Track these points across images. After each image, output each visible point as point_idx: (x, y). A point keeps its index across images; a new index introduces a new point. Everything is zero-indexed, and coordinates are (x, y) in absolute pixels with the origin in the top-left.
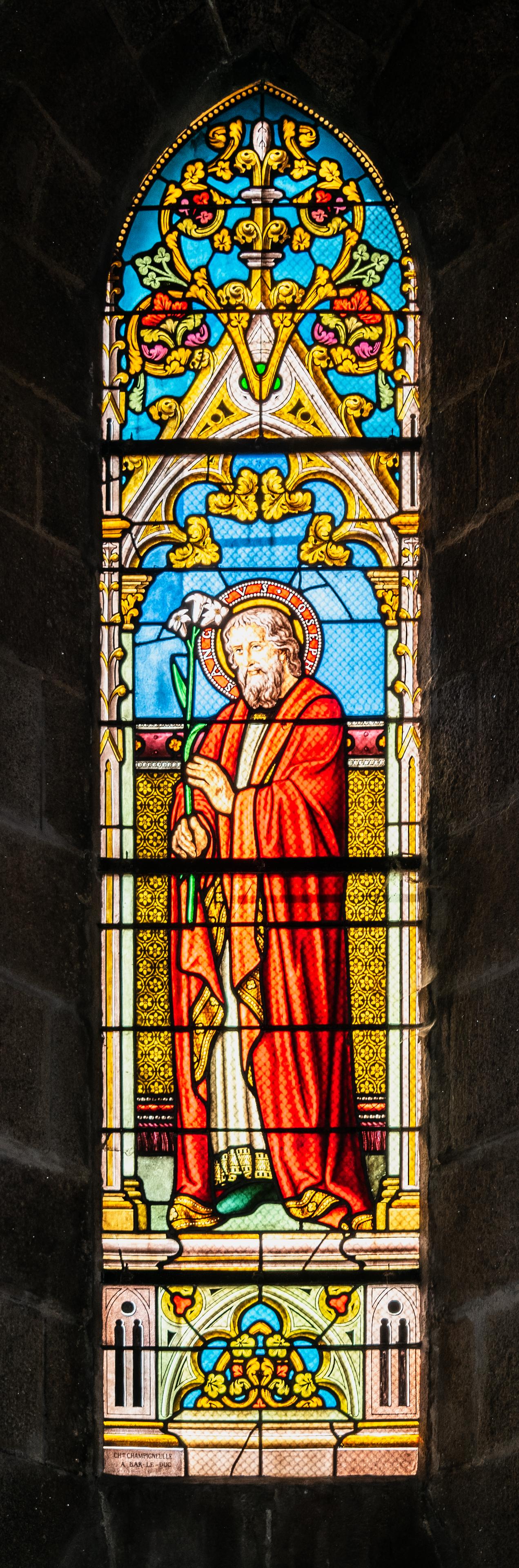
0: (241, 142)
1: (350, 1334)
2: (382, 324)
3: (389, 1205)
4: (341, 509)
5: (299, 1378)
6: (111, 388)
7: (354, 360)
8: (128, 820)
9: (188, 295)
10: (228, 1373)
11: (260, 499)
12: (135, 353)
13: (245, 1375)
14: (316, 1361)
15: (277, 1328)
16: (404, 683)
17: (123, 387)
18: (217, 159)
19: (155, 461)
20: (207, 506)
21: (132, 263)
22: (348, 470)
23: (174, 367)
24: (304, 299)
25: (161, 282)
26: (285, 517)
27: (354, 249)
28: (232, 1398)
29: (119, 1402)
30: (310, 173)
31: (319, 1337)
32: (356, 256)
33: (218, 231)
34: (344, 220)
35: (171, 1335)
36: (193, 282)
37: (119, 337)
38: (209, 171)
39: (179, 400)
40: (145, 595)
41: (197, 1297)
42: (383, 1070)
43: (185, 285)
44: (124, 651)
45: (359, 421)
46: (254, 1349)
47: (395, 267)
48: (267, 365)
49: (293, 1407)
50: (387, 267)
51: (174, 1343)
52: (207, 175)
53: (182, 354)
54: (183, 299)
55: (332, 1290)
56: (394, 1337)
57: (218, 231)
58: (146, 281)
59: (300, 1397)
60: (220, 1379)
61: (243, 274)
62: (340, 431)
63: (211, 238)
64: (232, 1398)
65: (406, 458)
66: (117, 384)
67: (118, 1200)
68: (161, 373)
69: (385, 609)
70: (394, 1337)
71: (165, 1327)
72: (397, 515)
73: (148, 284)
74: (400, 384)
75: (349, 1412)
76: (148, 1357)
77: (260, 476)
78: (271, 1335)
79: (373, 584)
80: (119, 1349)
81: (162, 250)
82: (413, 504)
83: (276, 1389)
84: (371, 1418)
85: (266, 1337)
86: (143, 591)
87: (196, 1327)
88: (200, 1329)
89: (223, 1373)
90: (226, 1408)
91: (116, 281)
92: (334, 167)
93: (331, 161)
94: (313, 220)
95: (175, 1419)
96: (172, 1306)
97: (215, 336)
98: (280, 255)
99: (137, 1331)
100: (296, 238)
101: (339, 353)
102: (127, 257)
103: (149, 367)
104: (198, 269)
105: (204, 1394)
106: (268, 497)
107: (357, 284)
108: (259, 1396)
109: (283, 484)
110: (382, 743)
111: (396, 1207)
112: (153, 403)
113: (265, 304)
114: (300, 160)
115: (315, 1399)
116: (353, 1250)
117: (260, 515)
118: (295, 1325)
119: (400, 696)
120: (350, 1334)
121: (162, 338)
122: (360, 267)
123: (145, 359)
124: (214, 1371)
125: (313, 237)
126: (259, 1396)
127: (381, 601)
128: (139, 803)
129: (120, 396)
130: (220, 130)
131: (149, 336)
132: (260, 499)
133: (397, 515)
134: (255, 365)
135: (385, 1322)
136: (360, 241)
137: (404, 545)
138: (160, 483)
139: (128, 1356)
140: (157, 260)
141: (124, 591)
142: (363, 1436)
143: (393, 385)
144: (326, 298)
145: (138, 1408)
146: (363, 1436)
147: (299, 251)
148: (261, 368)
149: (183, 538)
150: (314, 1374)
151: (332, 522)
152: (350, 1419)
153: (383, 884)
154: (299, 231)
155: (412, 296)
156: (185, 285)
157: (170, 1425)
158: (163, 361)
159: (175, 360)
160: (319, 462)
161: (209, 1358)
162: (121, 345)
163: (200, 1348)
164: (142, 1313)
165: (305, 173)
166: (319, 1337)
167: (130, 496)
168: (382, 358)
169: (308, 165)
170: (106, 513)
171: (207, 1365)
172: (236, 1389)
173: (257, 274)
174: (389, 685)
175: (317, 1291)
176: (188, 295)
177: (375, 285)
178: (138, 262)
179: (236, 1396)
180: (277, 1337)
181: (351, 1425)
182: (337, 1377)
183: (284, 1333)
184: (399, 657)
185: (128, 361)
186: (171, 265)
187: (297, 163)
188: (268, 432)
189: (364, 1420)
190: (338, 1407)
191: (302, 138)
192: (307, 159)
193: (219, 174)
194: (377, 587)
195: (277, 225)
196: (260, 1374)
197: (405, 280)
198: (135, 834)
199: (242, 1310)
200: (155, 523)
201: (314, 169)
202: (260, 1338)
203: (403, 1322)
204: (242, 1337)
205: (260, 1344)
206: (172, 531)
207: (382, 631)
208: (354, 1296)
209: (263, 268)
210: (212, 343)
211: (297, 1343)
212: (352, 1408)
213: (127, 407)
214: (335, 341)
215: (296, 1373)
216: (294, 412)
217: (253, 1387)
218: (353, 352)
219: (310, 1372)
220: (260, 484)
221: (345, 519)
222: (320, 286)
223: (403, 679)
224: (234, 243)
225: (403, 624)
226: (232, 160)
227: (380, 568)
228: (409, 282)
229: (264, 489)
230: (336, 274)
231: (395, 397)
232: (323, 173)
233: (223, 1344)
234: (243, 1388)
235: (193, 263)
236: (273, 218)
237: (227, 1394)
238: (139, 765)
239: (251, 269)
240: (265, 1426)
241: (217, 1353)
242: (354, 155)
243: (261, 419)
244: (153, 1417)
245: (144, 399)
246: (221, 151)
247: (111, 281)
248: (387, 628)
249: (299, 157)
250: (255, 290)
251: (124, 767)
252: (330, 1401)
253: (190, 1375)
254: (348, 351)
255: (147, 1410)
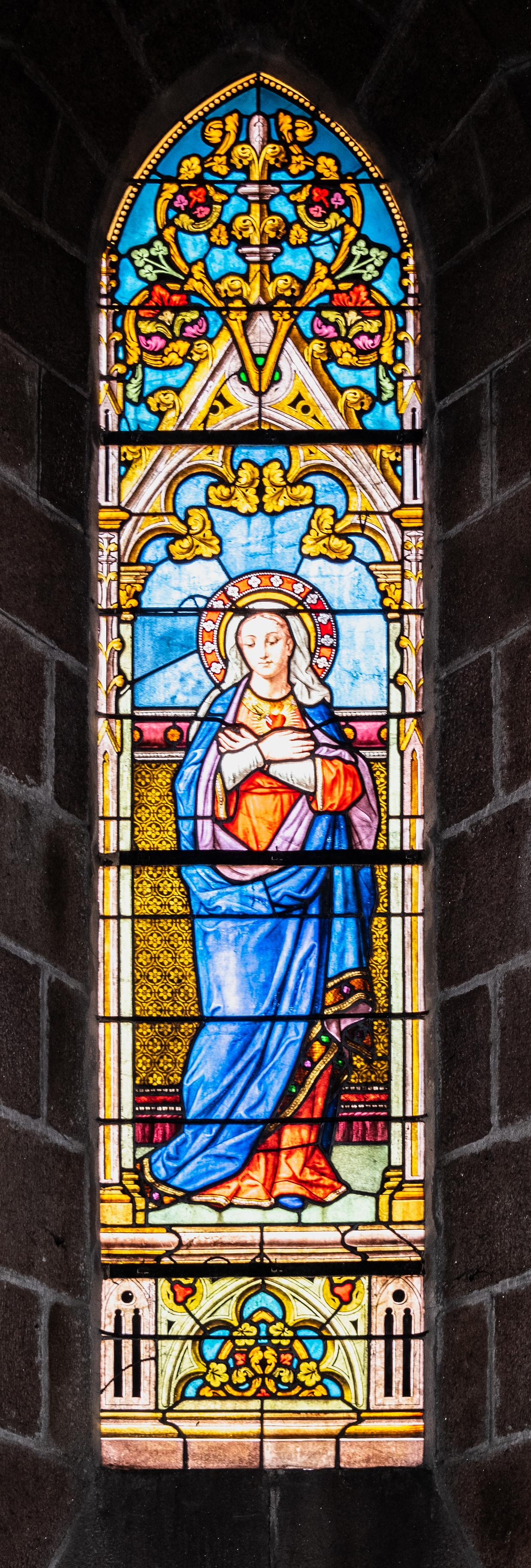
0: (238, 135)
1: (355, 1324)
2: (381, 317)
3: (392, 1198)
4: (343, 504)
5: (304, 1367)
6: (109, 378)
7: (354, 353)
8: (126, 812)
9: (187, 288)
10: (231, 1361)
11: (261, 491)
12: (133, 344)
13: (247, 1363)
14: (321, 1350)
15: (279, 1313)
16: (406, 675)
17: (121, 378)
18: (213, 154)
19: (157, 450)
20: (207, 498)
21: (128, 255)
22: (349, 463)
23: (174, 359)
24: (302, 293)
25: (158, 274)
26: (288, 509)
27: (353, 243)
28: (236, 1387)
29: (118, 1393)
30: (308, 168)
31: (323, 1326)
32: (354, 251)
33: (215, 226)
34: (342, 215)
35: (170, 1324)
36: (190, 275)
37: (115, 328)
38: (206, 166)
39: (178, 391)
40: (144, 586)
41: (197, 1285)
42: (385, 1048)
43: (182, 278)
44: (123, 642)
45: (360, 414)
46: (257, 1337)
47: (394, 261)
48: (265, 356)
49: (296, 1397)
50: (386, 261)
51: (173, 1332)
52: (204, 170)
53: (183, 346)
54: (181, 292)
55: (336, 1280)
56: (398, 1328)
57: (215, 226)
58: (142, 273)
59: (304, 1387)
60: (222, 1368)
61: (241, 267)
62: (339, 424)
63: (208, 233)
64: (236, 1387)
65: (408, 451)
66: (115, 375)
67: (117, 1194)
68: (160, 364)
69: (387, 602)
70: (398, 1328)
71: (165, 1315)
72: (399, 508)
73: (144, 276)
74: (400, 377)
75: (353, 1402)
76: (146, 1346)
77: (261, 469)
78: (274, 1323)
79: (375, 578)
80: (117, 1335)
81: (158, 244)
82: (415, 498)
83: (280, 1377)
84: (376, 1408)
85: (269, 1324)
86: (142, 581)
87: (198, 1316)
88: (201, 1318)
89: (226, 1362)
90: (229, 1397)
91: (113, 274)
92: (330, 162)
93: (328, 155)
94: (311, 217)
95: (176, 1408)
96: (171, 1294)
97: (213, 330)
98: (278, 250)
99: (136, 1320)
100: (293, 233)
101: (337, 347)
102: (123, 248)
103: (149, 359)
104: (195, 263)
105: (206, 1384)
106: (269, 490)
107: (356, 279)
108: (263, 1385)
109: (284, 477)
110: (383, 733)
111: (402, 1199)
112: (152, 394)
113: (264, 299)
114: (297, 155)
115: (320, 1387)
116: (356, 1242)
117: (261, 507)
118: (297, 1312)
119: (402, 689)
120: (355, 1324)
121: (160, 330)
122: (360, 262)
123: (142, 349)
124: (217, 1360)
125: (310, 232)
126: (263, 1385)
127: (384, 594)
128: (137, 794)
129: (118, 388)
130: (217, 124)
131: (147, 327)
132: (261, 491)
133: (399, 508)
134: (254, 356)
135: (389, 1311)
136: (359, 236)
137: (406, 538)
138: (163, 469)
139: (127, 1346)
140: (153, 252)
141: (122, 581)
142: (365, 1427)
143: (394, 378)
144: (326, 292)
145: (136, 1399)
146: (365, 1427)
147: (297, 246)
148: (260, 361)
149: (182, 529)
150: (318, 1362)
151: (334, 516)
152: (354, 1410)
153: (386, 873)
154: (297, 227)
155: (411, 290)
156: (182, 278)
157: (168, 1415)
158: (161, 352)
159: (173, 351)
160: (321, 454)
161: (211, 1349)
162: (118, 337)
163: (199, 1338)
164: (140, 1301)
165: (302, 168)
166: (323, 1326)
167: (129, 487)
168: (382, 351)
169: (306, 160)
170: (103, 503)
171: (210, 1354)
172: (240, 1377)
173: (255, 268)
174: (391, 677)
175: (321, 1282)
176: (187, 288)
177: (374, 279)
178: (134, 255)
179: (239, 1384)
180: (279, 1325)
181: (353, 1415)
182: (341, 1368)
183: (287, 1321)
184: (401, 650)
185: (126, 352)
186: (168, 258)
187: (295, 159)
188: (266, 422)
189: (368, 1410)
190: (342, 1398)
191: (299, 133)
192: (305, 154)
193: (215, 169)
194: (379, 580)
195: (274, 221)
196: (263, 1363)
197: (405, 275)
198: (133, 826)
199: (244, 1298)
200: (154, 514)
201: (312, 164)
202: (263, 1326)
203: (407, 1311)
204: (243, 1327)
205: (263, 1333)
206: (172, 522)
207: (383, 623)
208: (358, 1284)
209: (262, 262)
210: (210, 335)
211: (302, 1333)
212: (356, 1398)
213: (126, 399)
214: (336, 334)
215: (300, 1361)
216: (293, 404)
217: (256, 1376)
218: (353, 345)
219: (315, 1360)
220: (261, 476)
221: (347, 512)
222: (319, 280)
223: (405, 672)
224: (231, 238)
225: (405, 617)
226: (228, 154)
227: (383, 562)
228: (407, 276)
229: (266, 482)
230: (335, 268)
231: (395, 391)
232: (320, 169)
233: (226, 1333)
234: (247, 1377)
235: (192, 255)
236: (270, 213)
237: (230, 1382)
238: (136, 754)
239: (248, 263)
240: (266, 1415)
241: (218, 1344)
242: (351, 149)
243: (260, 411)
244: (152, 1407)
245: (142, 389)
246: (217, 146)
247: (107, 274)
248: (389, 621)
249: (296, 153)
250: (252, 284)
251: (122, 758)
252: (335, 1390)
253: (190, 1365)
254: (348, 345)
255: (145, 1400)
